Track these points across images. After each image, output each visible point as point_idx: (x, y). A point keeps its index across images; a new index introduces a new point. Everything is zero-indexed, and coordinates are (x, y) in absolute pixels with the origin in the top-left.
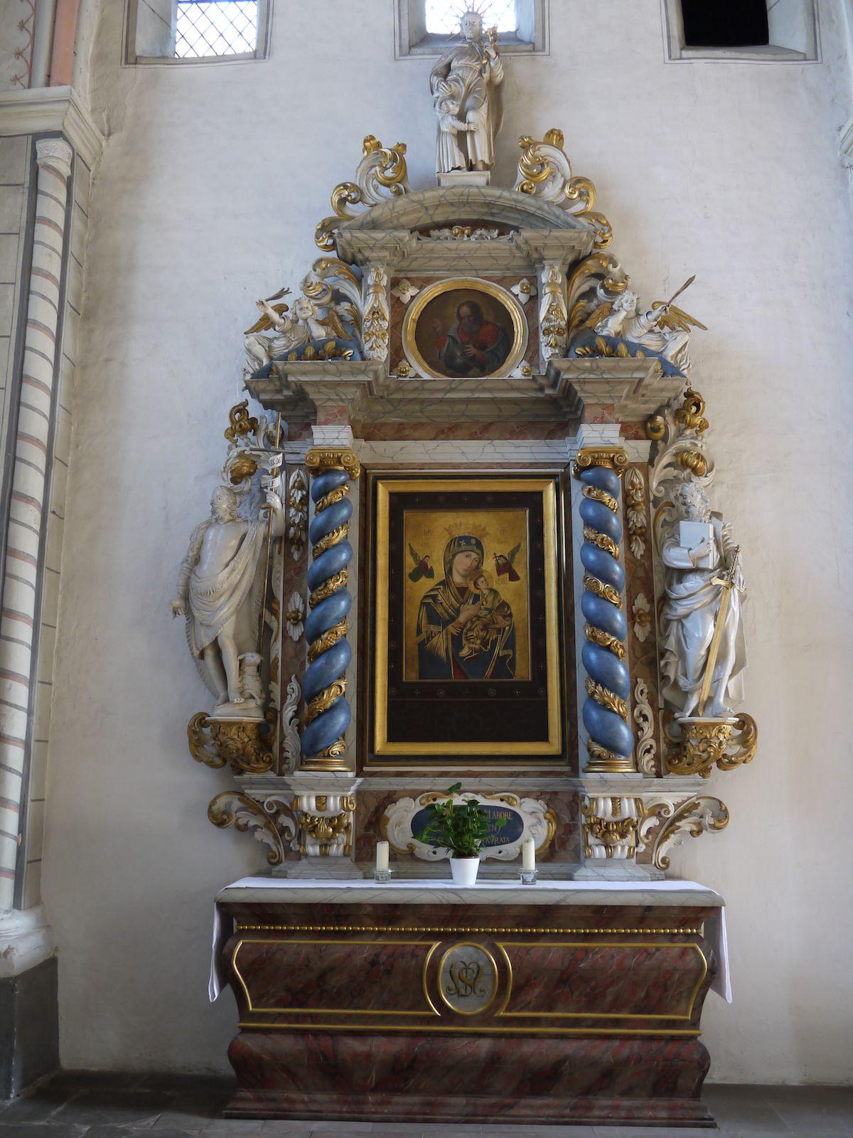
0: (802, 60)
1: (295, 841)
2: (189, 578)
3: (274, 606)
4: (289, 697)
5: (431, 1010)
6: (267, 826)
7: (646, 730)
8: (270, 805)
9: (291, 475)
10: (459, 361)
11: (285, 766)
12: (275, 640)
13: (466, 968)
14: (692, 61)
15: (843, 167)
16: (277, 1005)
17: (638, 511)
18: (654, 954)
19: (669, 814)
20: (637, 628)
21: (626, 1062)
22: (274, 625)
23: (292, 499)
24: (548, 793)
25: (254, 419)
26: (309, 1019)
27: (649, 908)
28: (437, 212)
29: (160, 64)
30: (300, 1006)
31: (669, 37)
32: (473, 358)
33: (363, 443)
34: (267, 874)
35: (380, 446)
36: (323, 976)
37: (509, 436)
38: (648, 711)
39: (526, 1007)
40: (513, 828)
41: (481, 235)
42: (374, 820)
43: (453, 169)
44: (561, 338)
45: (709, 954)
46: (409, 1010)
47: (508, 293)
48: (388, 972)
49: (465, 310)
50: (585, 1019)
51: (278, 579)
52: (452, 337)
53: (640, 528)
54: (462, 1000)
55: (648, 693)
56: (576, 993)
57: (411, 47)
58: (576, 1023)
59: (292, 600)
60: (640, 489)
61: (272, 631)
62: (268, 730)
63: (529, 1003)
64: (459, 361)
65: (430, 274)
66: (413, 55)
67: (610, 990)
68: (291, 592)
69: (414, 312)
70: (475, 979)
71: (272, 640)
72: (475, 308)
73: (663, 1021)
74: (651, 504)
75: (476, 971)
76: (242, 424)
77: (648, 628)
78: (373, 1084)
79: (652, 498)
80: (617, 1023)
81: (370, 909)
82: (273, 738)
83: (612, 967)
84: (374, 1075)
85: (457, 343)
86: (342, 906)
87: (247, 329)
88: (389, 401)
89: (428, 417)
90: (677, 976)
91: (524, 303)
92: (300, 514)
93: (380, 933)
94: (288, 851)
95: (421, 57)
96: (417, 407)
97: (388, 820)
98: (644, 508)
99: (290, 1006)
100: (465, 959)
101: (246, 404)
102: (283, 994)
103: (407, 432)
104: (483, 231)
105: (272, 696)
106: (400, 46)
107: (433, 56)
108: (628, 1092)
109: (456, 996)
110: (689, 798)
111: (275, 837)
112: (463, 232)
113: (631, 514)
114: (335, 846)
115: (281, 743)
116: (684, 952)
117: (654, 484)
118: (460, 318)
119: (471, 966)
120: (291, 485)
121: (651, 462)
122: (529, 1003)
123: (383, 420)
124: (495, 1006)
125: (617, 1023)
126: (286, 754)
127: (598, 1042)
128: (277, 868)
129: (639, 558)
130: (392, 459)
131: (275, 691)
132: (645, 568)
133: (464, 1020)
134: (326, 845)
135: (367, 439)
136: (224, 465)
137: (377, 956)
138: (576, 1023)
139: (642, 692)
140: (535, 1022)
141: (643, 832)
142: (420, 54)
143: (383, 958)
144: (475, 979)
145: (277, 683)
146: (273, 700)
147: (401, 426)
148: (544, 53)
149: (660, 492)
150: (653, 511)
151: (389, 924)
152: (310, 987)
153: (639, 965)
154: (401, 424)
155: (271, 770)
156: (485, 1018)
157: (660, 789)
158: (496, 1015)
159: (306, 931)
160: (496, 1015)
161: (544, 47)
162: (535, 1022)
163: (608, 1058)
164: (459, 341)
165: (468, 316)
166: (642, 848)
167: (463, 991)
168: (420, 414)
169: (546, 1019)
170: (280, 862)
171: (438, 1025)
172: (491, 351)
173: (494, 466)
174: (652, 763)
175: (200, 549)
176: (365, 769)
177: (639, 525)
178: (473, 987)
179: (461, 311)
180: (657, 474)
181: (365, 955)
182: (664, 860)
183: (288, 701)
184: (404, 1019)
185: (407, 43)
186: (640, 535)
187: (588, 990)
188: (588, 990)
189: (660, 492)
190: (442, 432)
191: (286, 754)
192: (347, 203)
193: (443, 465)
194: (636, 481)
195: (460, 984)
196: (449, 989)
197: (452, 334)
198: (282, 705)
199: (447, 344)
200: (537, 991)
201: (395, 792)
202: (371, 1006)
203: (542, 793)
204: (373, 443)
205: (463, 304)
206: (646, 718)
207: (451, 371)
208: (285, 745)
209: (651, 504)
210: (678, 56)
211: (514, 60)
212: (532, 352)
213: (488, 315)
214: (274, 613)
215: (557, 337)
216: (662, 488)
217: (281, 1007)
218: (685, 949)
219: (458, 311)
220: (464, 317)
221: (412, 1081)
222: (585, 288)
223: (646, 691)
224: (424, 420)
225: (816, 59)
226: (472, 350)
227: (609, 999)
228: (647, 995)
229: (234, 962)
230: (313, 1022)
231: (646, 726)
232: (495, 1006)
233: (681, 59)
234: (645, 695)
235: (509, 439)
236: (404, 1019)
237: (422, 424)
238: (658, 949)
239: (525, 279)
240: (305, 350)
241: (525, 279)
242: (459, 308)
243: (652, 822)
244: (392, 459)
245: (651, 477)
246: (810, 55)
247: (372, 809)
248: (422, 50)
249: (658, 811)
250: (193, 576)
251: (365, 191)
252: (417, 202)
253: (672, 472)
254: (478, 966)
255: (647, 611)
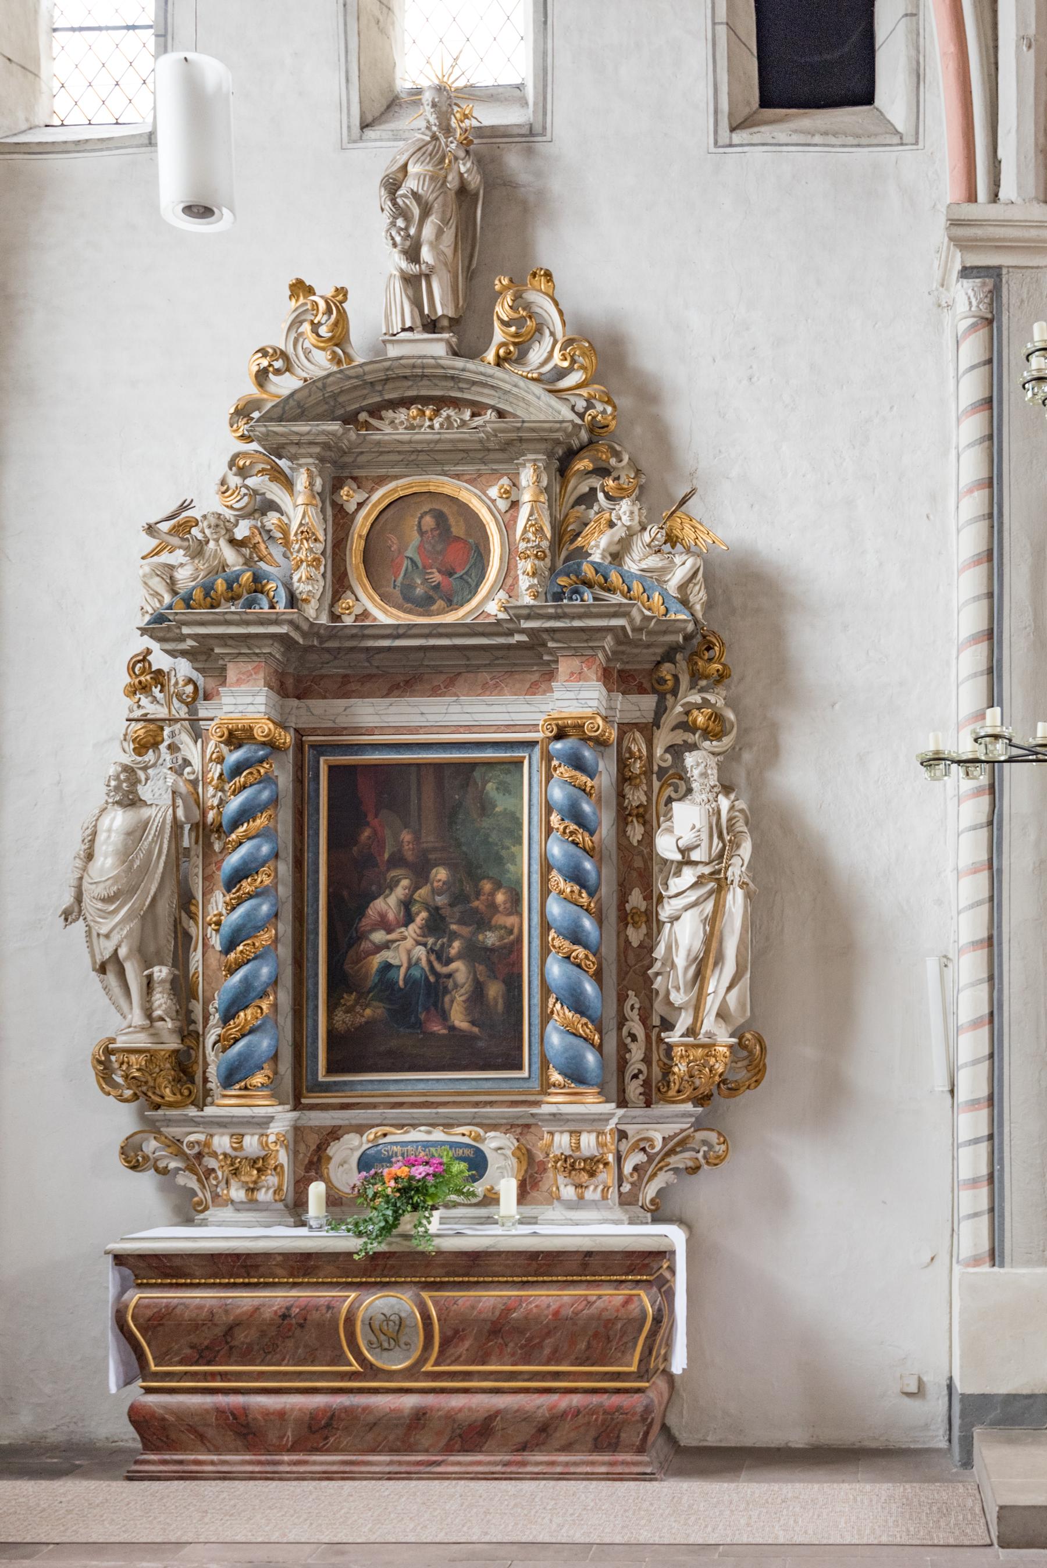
0: (898, 145)
1: (223, 1184)
2: (81, 878)
3: (193, 908)
4: (212, 1017)
5: (351, 1365)
6: (191, 1169)
7: (634, 1051)
8: (191, 1145)
9: (208, 744)
10: (419, 591)
11: (209, 1099)
12: (195, 950)
13: (387, 1319)
14: (746, 149)
15: (939, 306)
16: (181, 1363)
17: (637, 787)
18: (595, 1302)
19: (653, 1148)
20: (630, 931)
21: (564, 1415)
22: (193, 931)
23: (210, 775)
24: (518, 1126)
25: (159, 672)
26: (219, 1377)
27: (589, 1254)
28: (387, 387)
29: (20, 153)
30: (208, 1364)
31: (716, 112)
32: (437, 587)
33: (295, 702)
34: (189, 1221)
35: (318, 706)
36: (230, 1330)
37: (480, 691)
38: (639, 1030)
39: (456, 1361)
40: (478, 1164)
41: (448, 417)
42: (315, 1159)
43: (404, 330)
44: (542, 563)
45: (655, 1301)
46: (329, 1365)
47: (484, 497)
48: (301, 1326)
49: (429, 521)
50: (521, 1373)
51: (197, 875)
52: (411, 559)
53: (637, 807)
54: (385, 1354)
55: (639, 1009)
56: (511, 1345)
57: (365, 126)
58: (512, 1376)
59: (213, 900)
60: (640, 758)
61: (191, 938)
62: (190, 1055)
63: (460, 1356)
64: (419, 591)
65: (383, 471)
66: (367, 141)
67: (547, 1341)
68: (212, 891)
69: (361, 524)
70: (398, 1331)
71: (192, 949)
72: (440, 518)
73: (606, 1373)
74: (655, 776)
75: (397, 1322)
76: (146, 679)
77: (644, 929)
78: (290, 1443)
79: (656, 768)
80: (556, 1376)
81: (279, 1258)
82: (195, 1068)
83: (547, 1316)
84: (289, 1433)
85: (417, 567)
86: (248, 1256)
87: (144, 554)
88: (328, 650)
89: (378, 667)
90: (619, 1326)
91: (503, 511)
92: (220, 794)
93: (295, 1285)
94: (216, 1196)
95: (378, 144)
96: (363, 656)
97: (330, 1158)
98: (644, 781)
99: (196, 1364)
100: (385, 1311)
101: (149, 652)
102: (188, 1351)
103: (353, 686)
104: (451, 412)
105: (193, 1017)
106: (349, 127)
107: (392, 144)
108: (567, 1448)
109: (378, 1350)
110: (683, 1131)
111: (199, 1180)
112: (424, 413)
113: (627, 789)
114: (264, 1190)
115: (204, 1072)
116: (628, 1300)
117: (659, 752)
118: (421, 533)
119: (392, 1318)
120: (208, 757)
121: (656, 723)
122: (460, 1356)
123: (324, 672)
124: (422, 1360)
125: (556, 1376)
126: (209, 1085)
127: (536, 1396)
128: (201, 1216)
129: (635, 844)
130: (334, 722)
131: (196, 1012)
132: (643, 856)
133: (391, 1375)
134: (253, 1190)
135: (299, 698)
136: (124, 732)
137: (288, 1308)
138: (512, 1376)
139: (632, 1008)
140: (467, 1376)
141: (628, 1168)
142: (376, 140)
143: (295, 1311)
144: (398, 1331)
145: (198, 1001)
146: (194, 1022)
147: (346, 679)
148: (544, 139)
149: (665, 761)
150: (656, 784)
151: (304, 1275)
152: (217, 1343)
153: (577, 1314)
154: (346, 676)
155: (192, 1103)
156: (411, 1373)
157: (647, 1120)
158: (423, 1370)
159: (432, 1282)
160: (423, 1370)
161: (544, 128)
162: (467, 1376)
163: (543, 1413)
164: (420, 565)
165: (432, 530)
166: (626, 1188)
167: (386, 1345)
168: (367, 664)
169: (479, 1372)
170: (206, 1209)
171: (360, 1381)
172: (461, 577)
173: (462, 730)
174: (641, 1090)
175: (92, 841)
176: (303, 1101)
177: (634, 804)
178: (397, 1341)
179: (423, 521)
180: (663, 739)
181: (275, 1308)
182: (652, 1201)
183: (211, 1023)
184: (322, 1376)
185: (358, 124)
186: (638, 816)
187: (523, 1342)
188: (523, 1342)
189: (665, 761)
190: (397, 686)
191: (209, 1085)
192: (271, 375)
193: (398, 730)
194: (634, 748)
195: (382, 1337)
196: (370, 1343)
197: (410, 555)
198: (204, 1027)
199: (404, 569)
200: (467, 1344)
201: (340, 1127)
202: (286, 1362)
203: (512, 1126)
204: (311, 703)
205: (426, 513)
206: (634, 1038)
207: (409, 605)
208: (208, 1075)
209: (655, 776)
210: (727, 142)
211: (503, 149)
212: (507, 580)
213: (458, 529)
214: (192, 916)
215: (536, 562)
216: (668, 756)
217: (186, 1365)
218: (631, 1295)
219: (419, 523)
220: (426, 532)
221: (332, 1440)
222: (584, 488)
223: (637, 1006)
224: (375, 671)
225: (917, 143)
226: (437, 577)
227: (547, 1351)
228: (589, 1347)
229: (130, 1319)
230: (222, 1381)
231: (633, 1046)
232: (422, 1360)
233: (731, 145)
234: (636, 1011)
235: (479, 695)
236: (322, 1376)
237: (370, 677)
238: (600, 1297)
239: (505, 478)
240: (213, 584)
241: (505, 478)
242: (421, 518)
243: (639, 1158)
244: (334, 722)
245: (655, 741)
246: (909, 138)
247: (314, 1147)
248: (378, 133)
249: (642, 1146)
250: (86, 876)
251: (292, 357)
252: (357, 377)
253: (679, 737)
254: (400, 1318)
255: (643, 909)
